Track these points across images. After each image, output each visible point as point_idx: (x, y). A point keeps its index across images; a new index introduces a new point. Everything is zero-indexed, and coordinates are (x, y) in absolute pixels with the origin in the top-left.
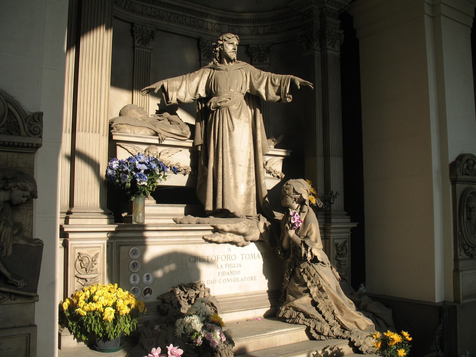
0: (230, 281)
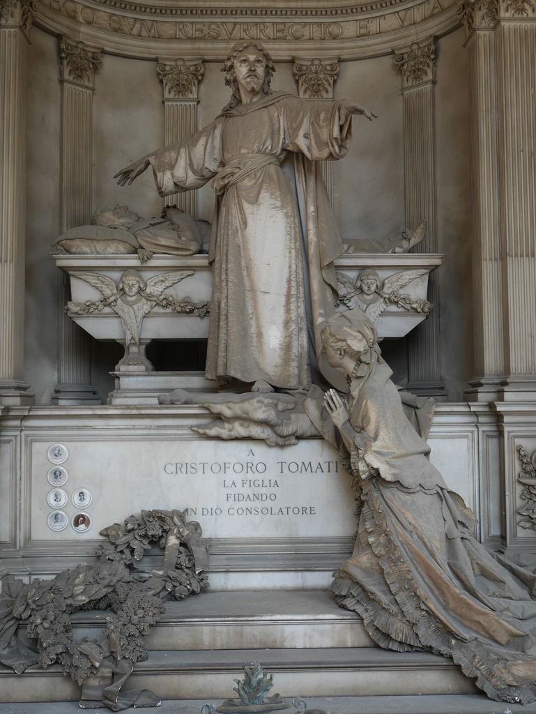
0: (253, 511)
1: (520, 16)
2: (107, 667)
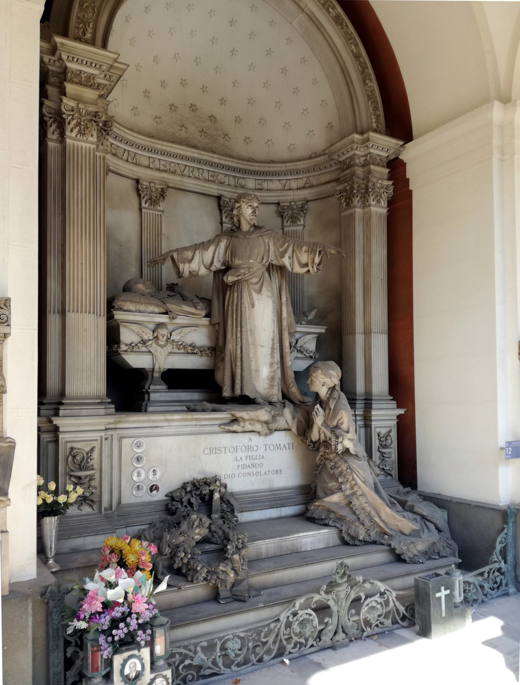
0: (251, 475)
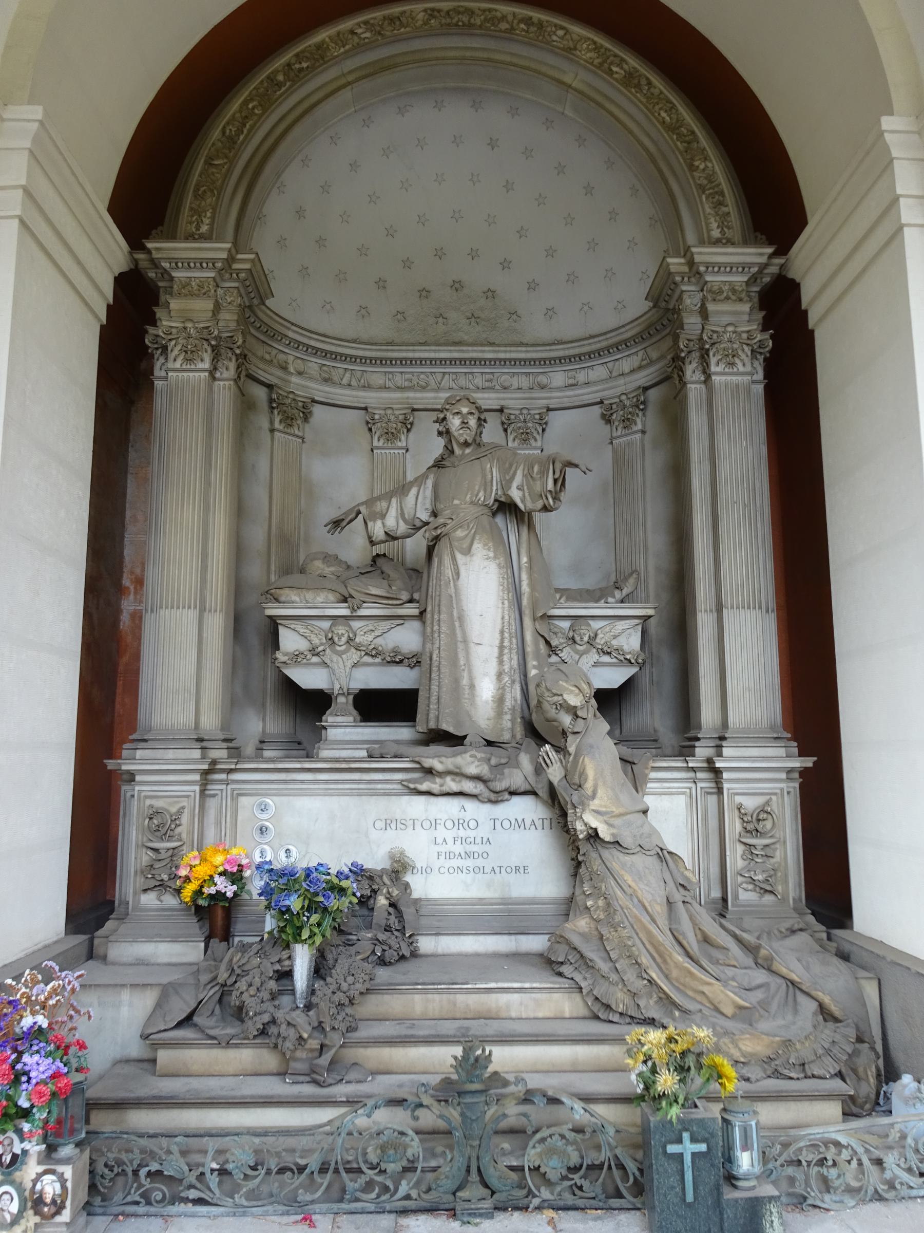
0: (465, 870)
1: (731, 370)
2: (315, 1038)
